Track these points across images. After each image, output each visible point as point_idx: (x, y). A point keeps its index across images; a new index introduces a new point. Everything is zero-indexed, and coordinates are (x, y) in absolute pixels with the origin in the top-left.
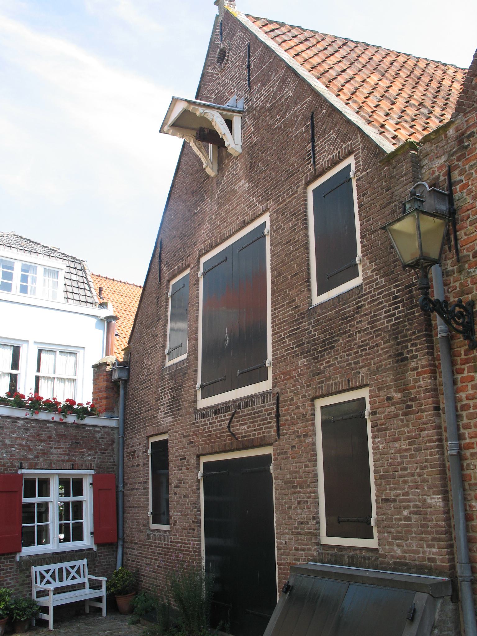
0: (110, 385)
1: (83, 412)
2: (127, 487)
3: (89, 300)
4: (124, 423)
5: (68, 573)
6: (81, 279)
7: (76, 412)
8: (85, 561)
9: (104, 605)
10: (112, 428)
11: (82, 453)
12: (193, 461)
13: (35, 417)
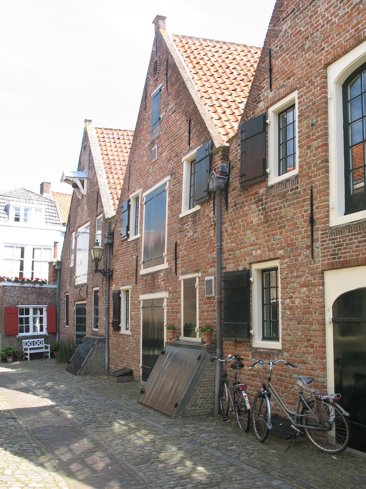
0: (55, 271)
1: (43, 283)
2: (61, 312)
3: (58, 222)
4: (59, 286)
5: (36, 343)
6: (54, 212)
7: (39, 283)
8: (43, 339)
9: (49, 355)
10: (55, 288)
12: (73, 303)
13: (23, 286)
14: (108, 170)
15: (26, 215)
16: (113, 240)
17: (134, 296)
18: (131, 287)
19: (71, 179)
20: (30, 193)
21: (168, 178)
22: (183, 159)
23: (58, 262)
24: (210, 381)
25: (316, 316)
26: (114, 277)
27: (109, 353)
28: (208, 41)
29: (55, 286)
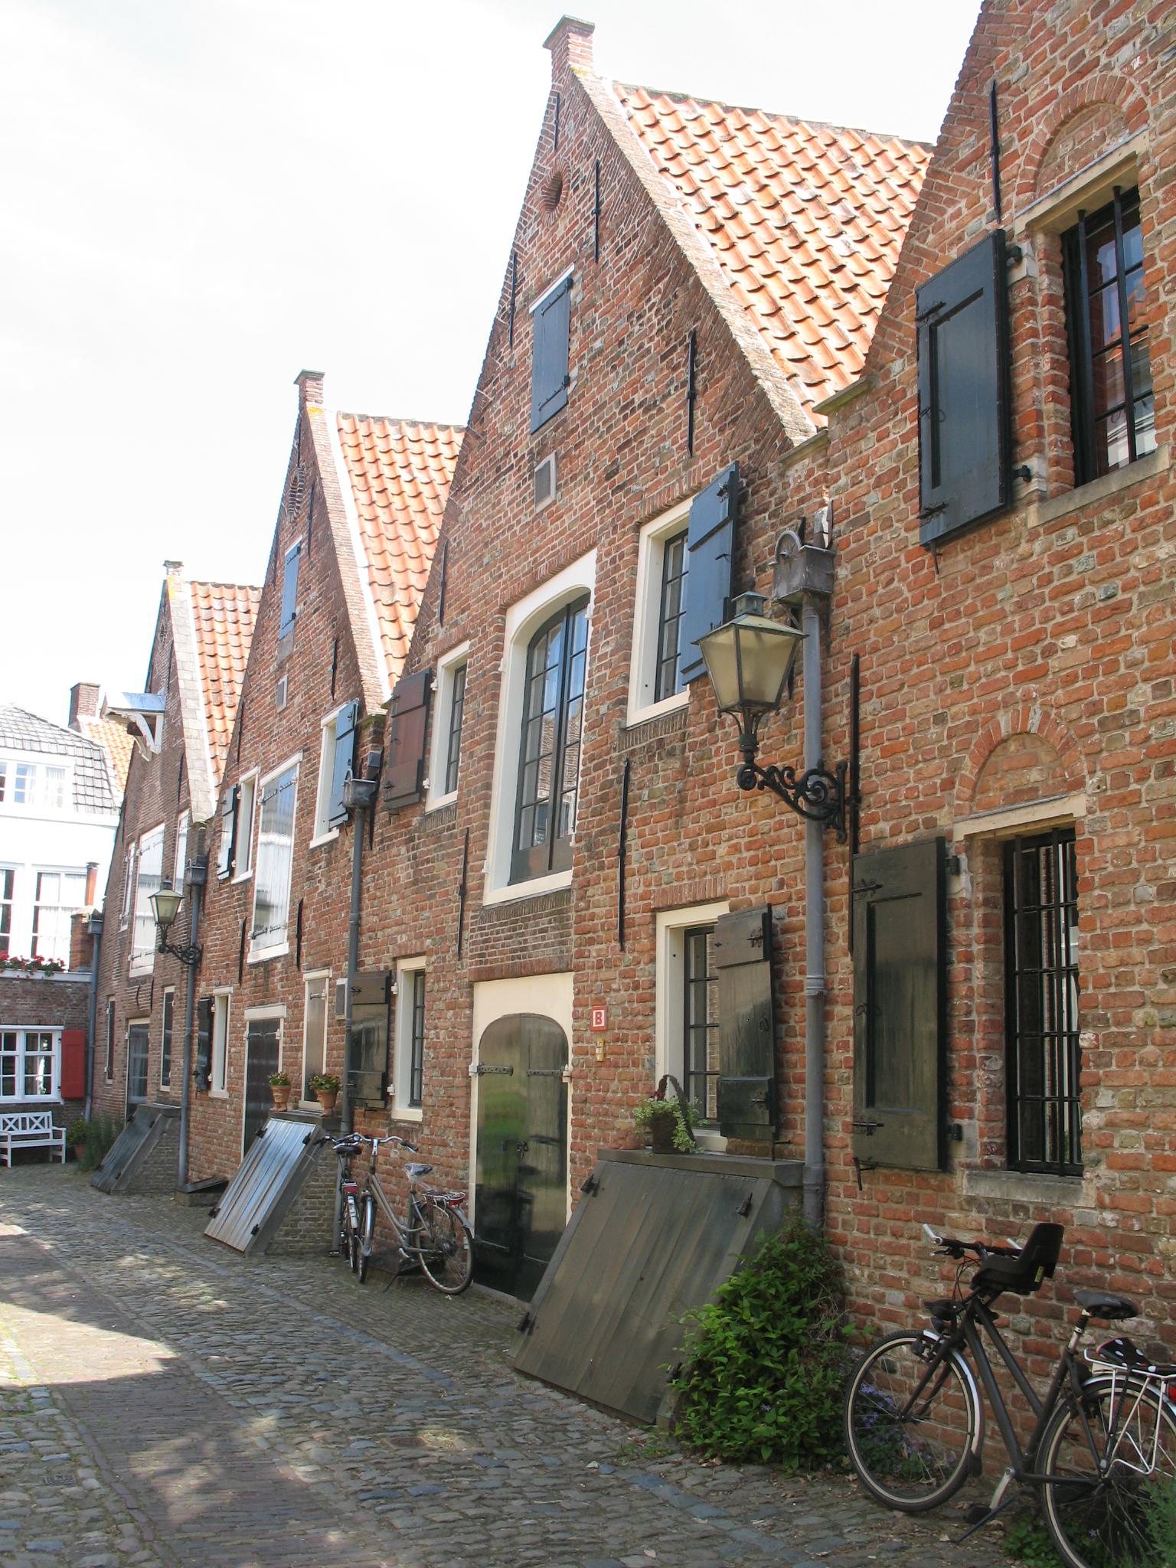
1: (55, 968)
3: (108, 803)
5: (32, 1123)
6: (98, 774)
7: (45, 968)
9: (63, 1154)
11: (51, 1009)
14: (212, 697)
15: (20, 783)
16: (206, 875)
17: (237, 1011)
18: (231, 989)
19: (123, 714)
20: (35, 721)
21: (298, 757)
22: (324, 721)
23: (95, 916)
24: (327, 1186)
25: (459, 1062)
26: (205, 962)
27: (188, 1145)
28: (421, 427)
29: (87, 979)
